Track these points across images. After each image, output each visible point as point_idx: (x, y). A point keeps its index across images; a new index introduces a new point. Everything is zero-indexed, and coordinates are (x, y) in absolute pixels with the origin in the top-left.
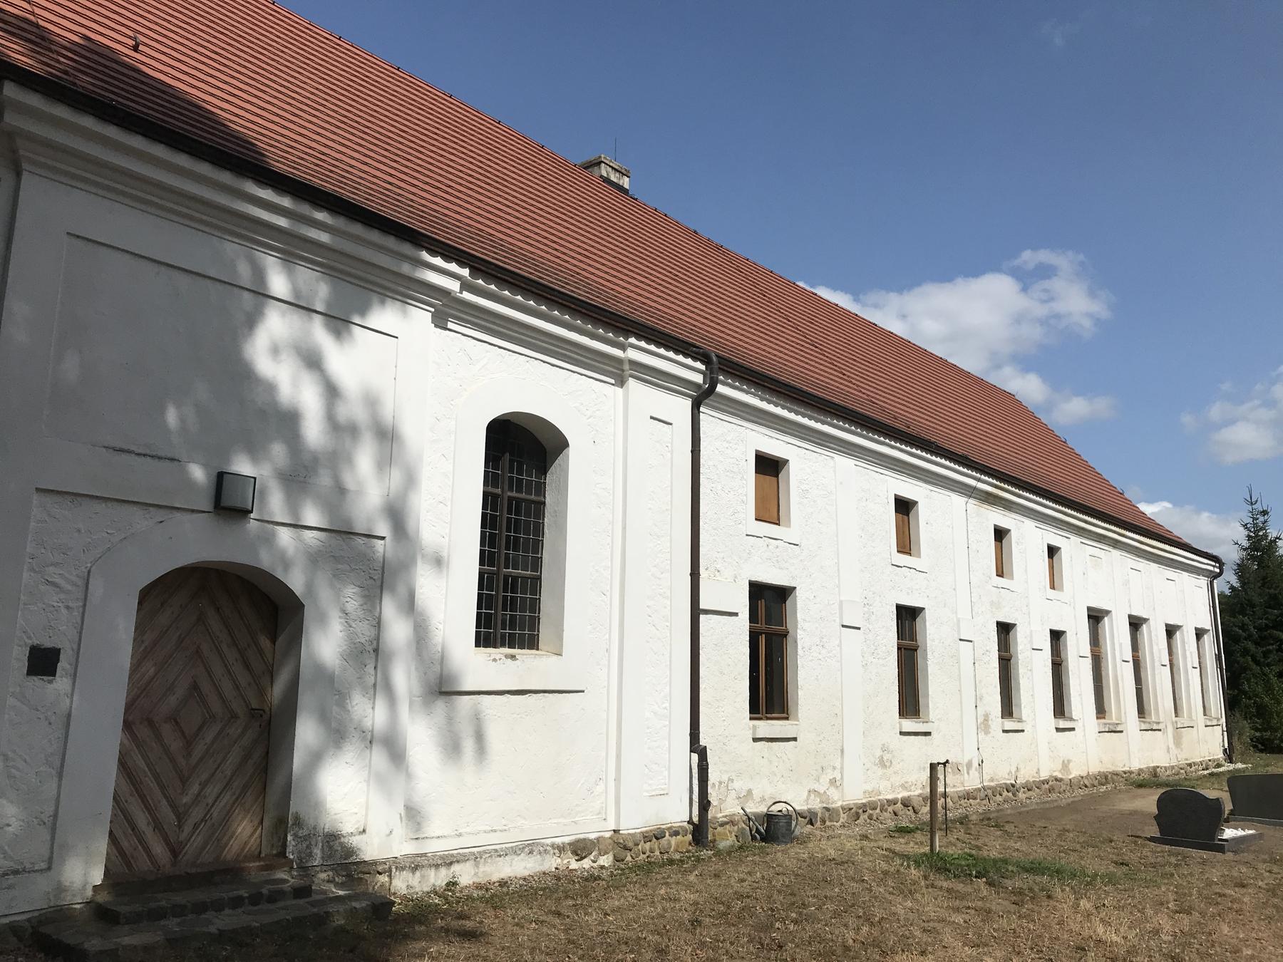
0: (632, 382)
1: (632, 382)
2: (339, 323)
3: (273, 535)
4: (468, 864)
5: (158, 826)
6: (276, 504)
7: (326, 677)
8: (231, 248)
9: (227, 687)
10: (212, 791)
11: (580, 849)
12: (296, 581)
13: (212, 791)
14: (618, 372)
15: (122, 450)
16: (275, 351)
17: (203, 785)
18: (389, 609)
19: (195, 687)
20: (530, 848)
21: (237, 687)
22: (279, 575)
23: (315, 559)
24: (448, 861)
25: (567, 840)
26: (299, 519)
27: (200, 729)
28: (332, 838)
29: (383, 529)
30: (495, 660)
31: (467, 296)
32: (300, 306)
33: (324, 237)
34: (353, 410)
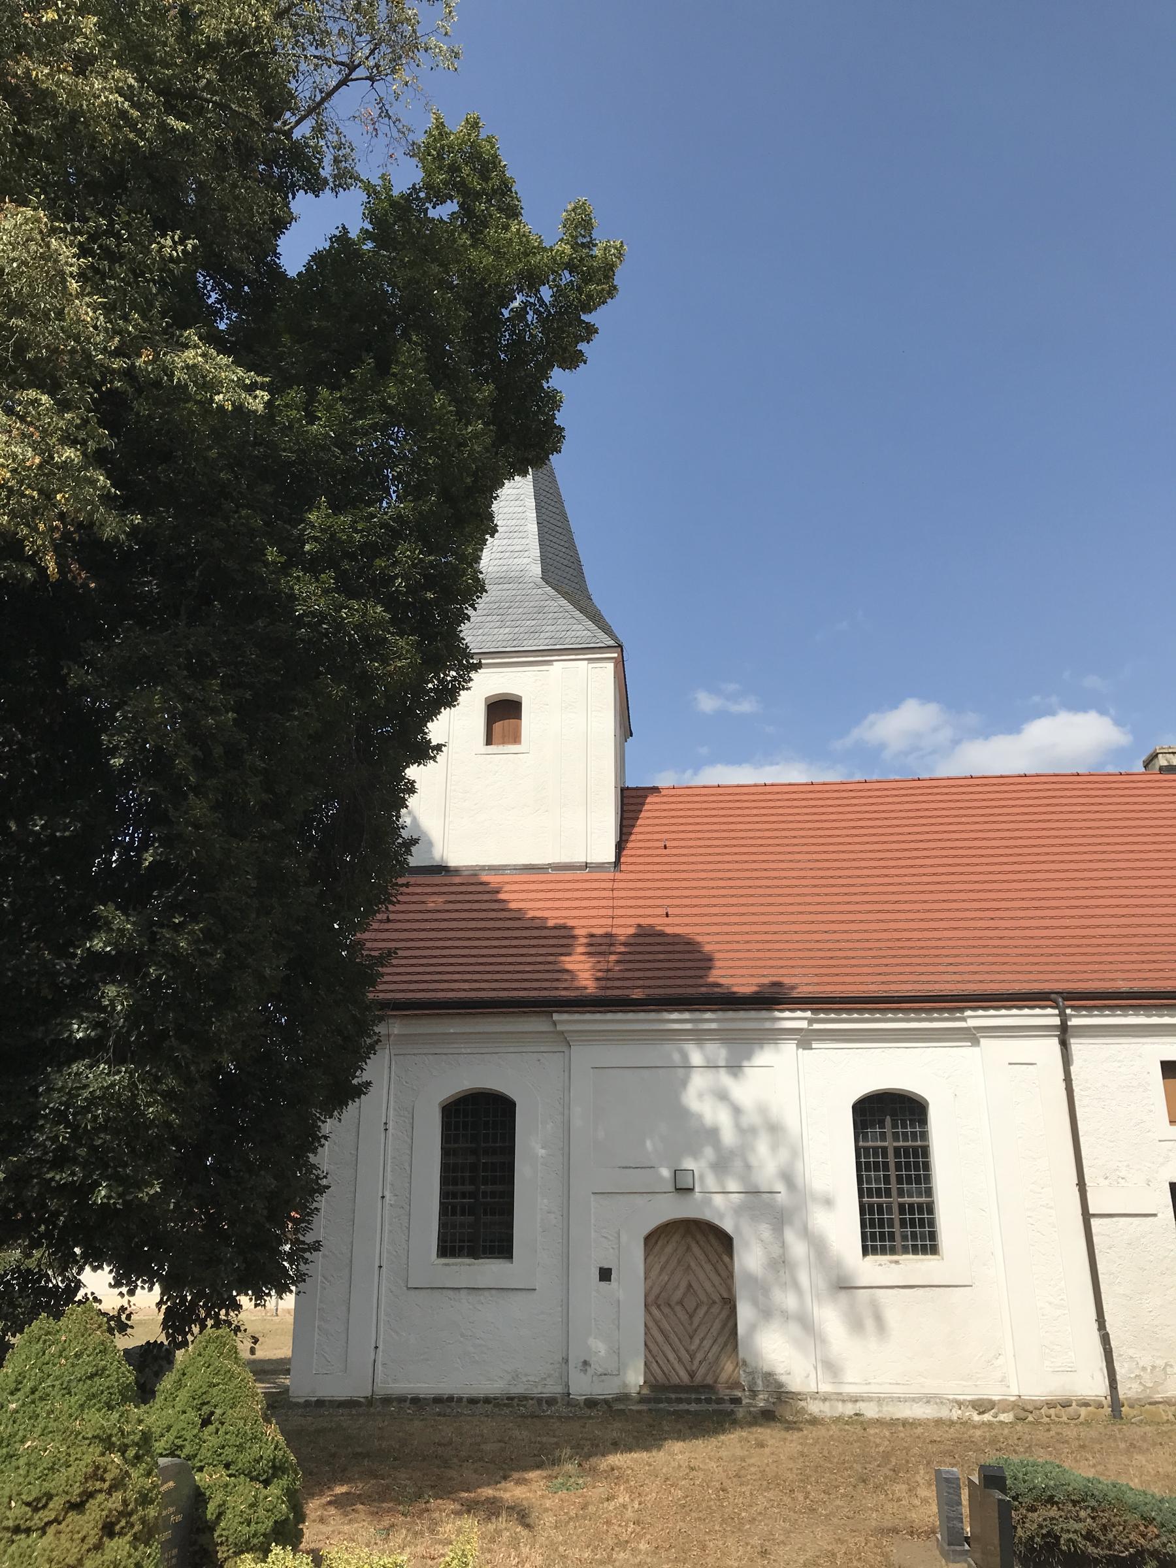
0: (982, 1041)
1: (982, 1041)
2: (735, 1068)
3: (710, 1199)
4: (872, 1403)
5: (680, 1360)
6: (711, 1183)
7: (752, 1279)
8: (668, 1047)
9: (708, 1286)
10: (707, 1343)
11: (982, 1406)
12: (728, 1226)
13: (707, 1343)
14: (972, 1036)
15: (626, 1168)
16: (700, 1096)
17: (702, 1340)
18: (790, 1236)
19: (690, 1286)
20: (928, 1400)
21: (714, 1286)
22: (717, 1222)
23: (739, 1211)
24: (855, 1400)
25: (969, 1398)
26: (724, 1188)
27: (695, 1309)
28: (769, 1376)
29: (780, 1187)
30: (880, 1265)
31: (816, 1026)
32: (712, 1066)
33: (714, 1026)
34: (751, 1118)
